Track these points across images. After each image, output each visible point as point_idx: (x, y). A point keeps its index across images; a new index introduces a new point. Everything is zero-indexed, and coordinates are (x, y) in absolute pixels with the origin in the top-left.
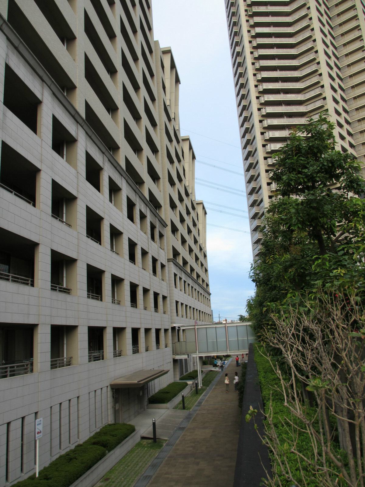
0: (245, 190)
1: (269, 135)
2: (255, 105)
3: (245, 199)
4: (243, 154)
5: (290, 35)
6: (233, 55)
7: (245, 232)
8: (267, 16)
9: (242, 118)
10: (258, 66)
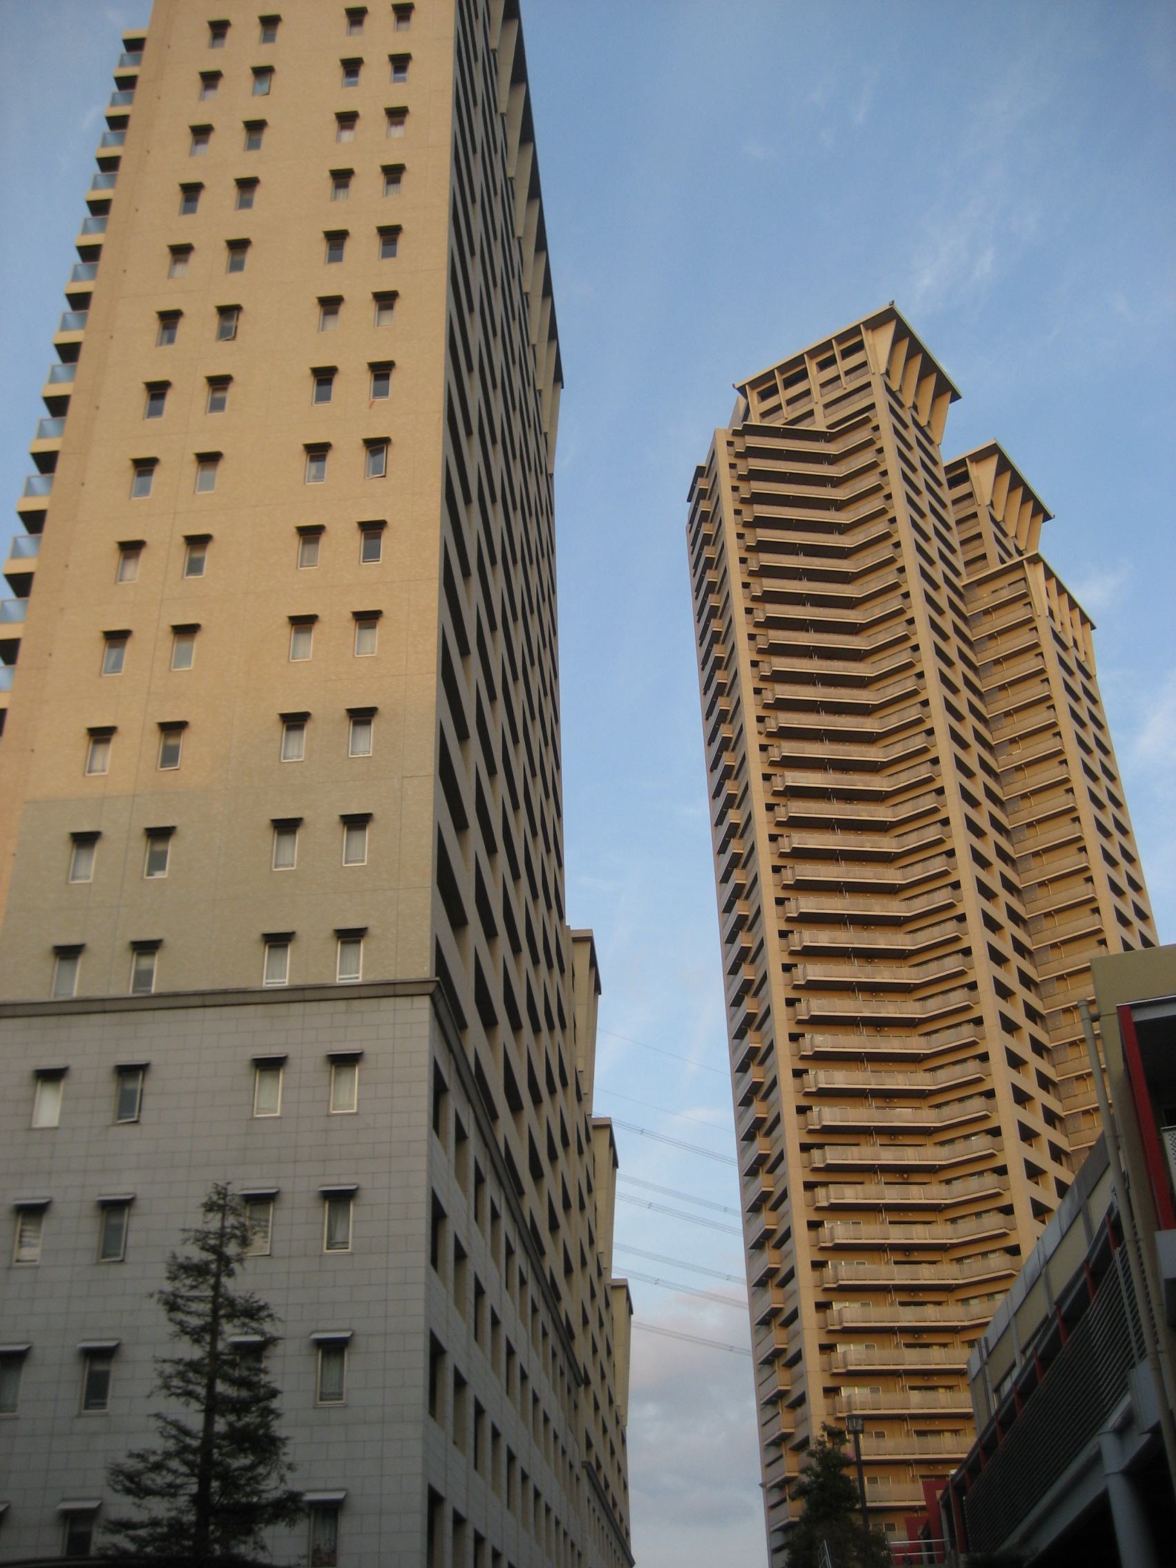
0: (742, 1274)
1: (801, 941)
2: (768, 889)
3: (737, 1222)
4: (725, 957)
5: (843, 553)
6: (702, 638)
7: (726, 1209)
8: (795, 579)
9: (726, 858)
10: (816, 1120)
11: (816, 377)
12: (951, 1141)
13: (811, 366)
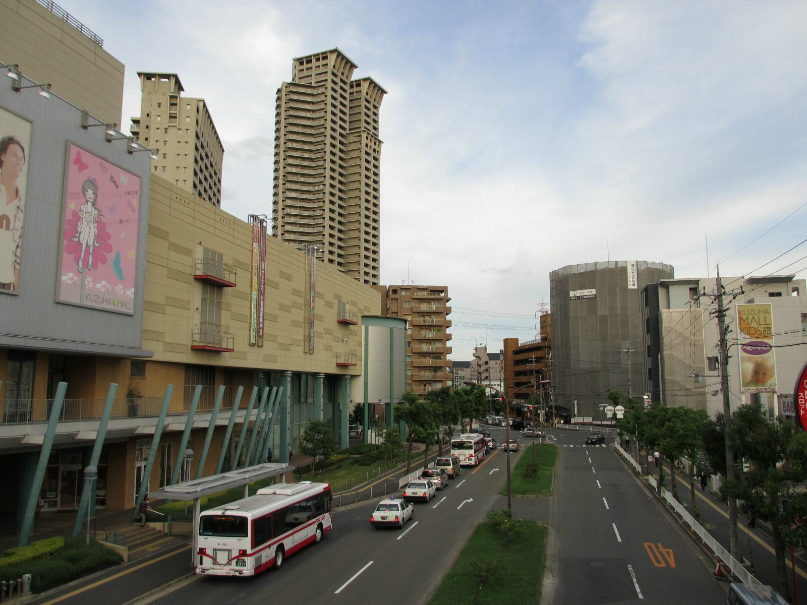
11: (314, 64)
12: (316, 169)
13: (314, 60)
